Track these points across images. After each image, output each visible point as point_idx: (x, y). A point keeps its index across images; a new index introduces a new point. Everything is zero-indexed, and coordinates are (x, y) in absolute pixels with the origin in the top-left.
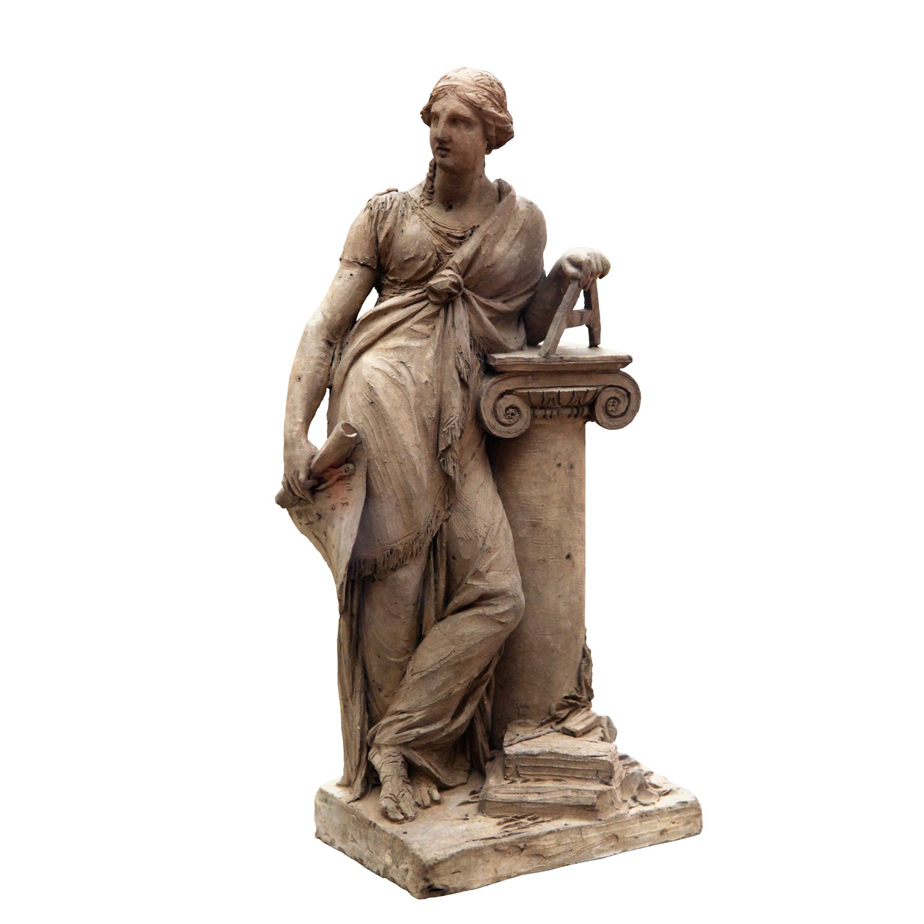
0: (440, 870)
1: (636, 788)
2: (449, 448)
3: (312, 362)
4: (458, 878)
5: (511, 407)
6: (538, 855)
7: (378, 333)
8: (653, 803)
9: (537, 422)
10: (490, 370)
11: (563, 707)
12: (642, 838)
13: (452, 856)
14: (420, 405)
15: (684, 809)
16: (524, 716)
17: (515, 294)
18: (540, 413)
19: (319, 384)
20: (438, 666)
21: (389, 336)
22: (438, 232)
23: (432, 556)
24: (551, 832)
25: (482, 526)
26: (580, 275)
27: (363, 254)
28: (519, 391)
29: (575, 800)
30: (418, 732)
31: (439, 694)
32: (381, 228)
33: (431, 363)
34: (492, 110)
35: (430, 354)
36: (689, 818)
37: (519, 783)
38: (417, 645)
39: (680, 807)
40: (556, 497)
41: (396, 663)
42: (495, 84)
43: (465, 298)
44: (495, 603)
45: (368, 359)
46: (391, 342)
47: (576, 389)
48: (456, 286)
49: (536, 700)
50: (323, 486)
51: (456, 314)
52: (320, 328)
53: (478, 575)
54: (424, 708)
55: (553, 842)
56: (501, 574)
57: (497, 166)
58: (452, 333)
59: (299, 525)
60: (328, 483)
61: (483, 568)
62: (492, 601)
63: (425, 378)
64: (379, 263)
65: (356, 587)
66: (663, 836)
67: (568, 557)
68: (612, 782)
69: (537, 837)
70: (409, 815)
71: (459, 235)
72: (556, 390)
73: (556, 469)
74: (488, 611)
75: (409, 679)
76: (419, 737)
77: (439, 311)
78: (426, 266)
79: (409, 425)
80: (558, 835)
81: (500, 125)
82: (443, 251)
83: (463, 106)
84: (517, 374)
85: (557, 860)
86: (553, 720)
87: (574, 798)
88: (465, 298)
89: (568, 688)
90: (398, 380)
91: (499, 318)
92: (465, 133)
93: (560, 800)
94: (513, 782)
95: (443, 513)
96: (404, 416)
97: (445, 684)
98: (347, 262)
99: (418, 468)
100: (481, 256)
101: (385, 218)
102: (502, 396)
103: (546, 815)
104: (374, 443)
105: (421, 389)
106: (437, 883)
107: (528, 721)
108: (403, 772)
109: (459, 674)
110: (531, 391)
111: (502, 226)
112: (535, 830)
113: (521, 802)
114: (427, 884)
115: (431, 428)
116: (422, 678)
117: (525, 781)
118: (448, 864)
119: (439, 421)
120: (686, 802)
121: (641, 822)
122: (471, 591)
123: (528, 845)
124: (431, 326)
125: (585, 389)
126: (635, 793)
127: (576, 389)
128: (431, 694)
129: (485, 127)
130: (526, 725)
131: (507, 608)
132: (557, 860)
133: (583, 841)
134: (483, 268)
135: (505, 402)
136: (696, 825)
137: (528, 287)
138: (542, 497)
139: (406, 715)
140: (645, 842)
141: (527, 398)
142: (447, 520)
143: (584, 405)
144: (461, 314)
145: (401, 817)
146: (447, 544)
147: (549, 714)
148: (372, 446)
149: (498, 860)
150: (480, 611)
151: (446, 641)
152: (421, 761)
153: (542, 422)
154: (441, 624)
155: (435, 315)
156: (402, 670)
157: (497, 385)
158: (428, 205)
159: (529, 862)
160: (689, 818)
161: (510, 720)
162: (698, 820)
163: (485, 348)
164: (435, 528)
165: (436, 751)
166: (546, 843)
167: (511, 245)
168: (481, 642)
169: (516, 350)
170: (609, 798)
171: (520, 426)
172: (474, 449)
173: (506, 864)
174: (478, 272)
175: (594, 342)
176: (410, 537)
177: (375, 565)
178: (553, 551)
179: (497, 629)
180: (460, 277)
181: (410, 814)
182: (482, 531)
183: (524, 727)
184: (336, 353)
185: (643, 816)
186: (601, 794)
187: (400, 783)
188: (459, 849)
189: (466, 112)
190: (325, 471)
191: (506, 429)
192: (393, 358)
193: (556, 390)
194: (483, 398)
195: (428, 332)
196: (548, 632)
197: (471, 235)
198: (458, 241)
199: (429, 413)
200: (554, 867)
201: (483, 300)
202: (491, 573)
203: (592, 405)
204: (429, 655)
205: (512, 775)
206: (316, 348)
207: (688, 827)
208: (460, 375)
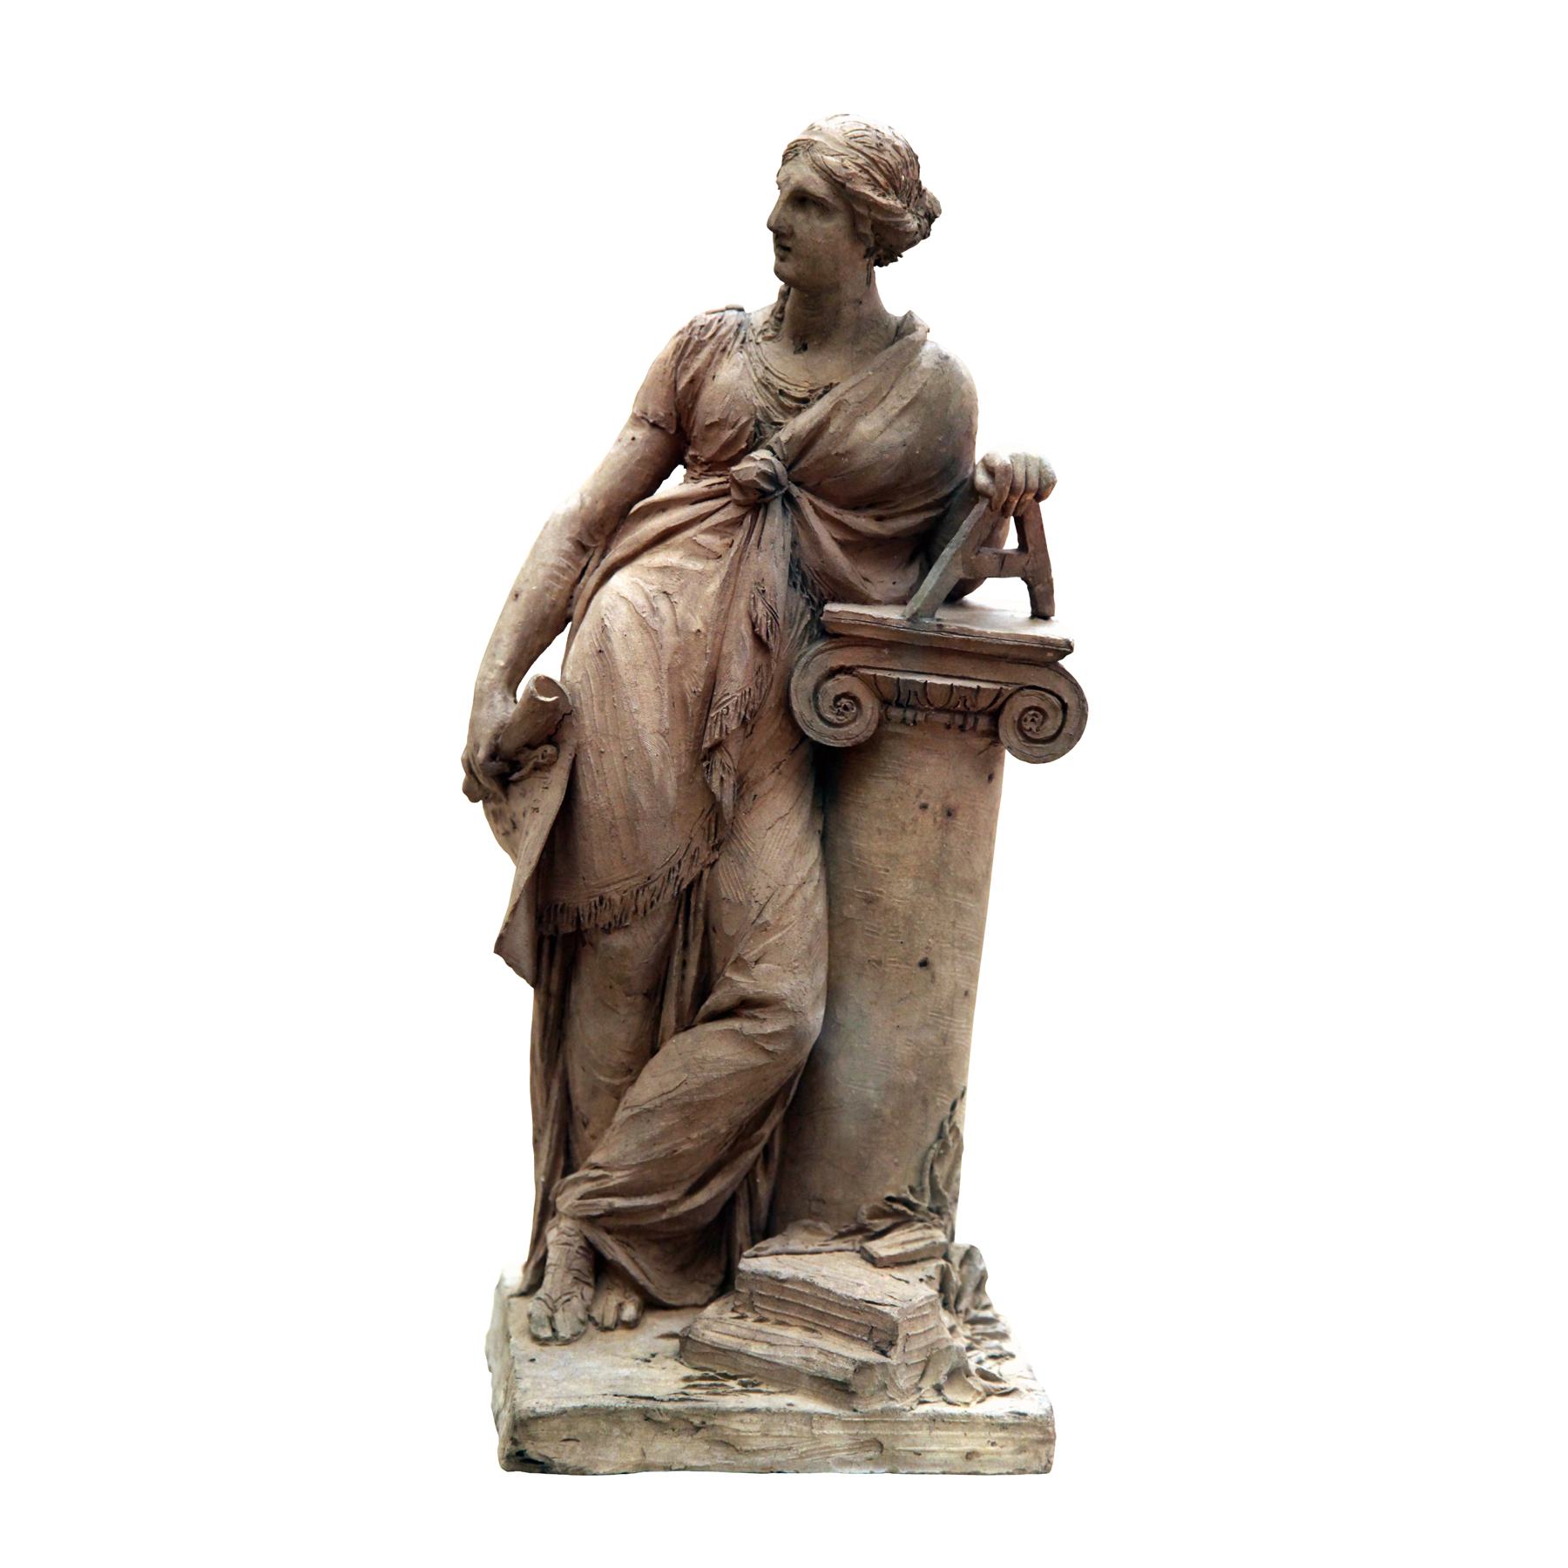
0: (540, 1429)
1: (946, 1370)
2: (717, 746)
3: (541, 572)
4: (573, 1450)
5: (845, 695)
6: (727, 1444)
7: (645, 540)
8: (967, 1404)
9: (891, 728)
10: (824, 632)
11: (878, 1213)
12: (929, 1456)
13: (564, 1411)
14: (681, 667)
15: (1019, 1425)
16: (816, 1216)
17: (904, 508)
18: (895, 713)
19: (547, 610)
20: (658, 1102)
21: (661, 546)
22: (766, 385)
23: (681, 921)
24: (752, 1411)
25: (763, 884)
26: (992, 490)
27: (658, 410)
28: (862, 671)
29: (820, 1368)
30: (610, 1204)
31: (656, 1149)
32: (686, 368)
33: (712, 601)
34: (867, 190)
35: (713, 586)
36: (1032, 1443)
37: (749, 1322)
38: (644, 1062)
39: (1010, 1420)
40: (912, 860)
41: (608, 1086)
42: (888, 146)
43: (789, 500)
44: (762, 1016)
45: (620, 580)
46: (660, 557)
47: (957, 683)
48: (772, 478)
49: (838, 1194)
50: (516, 776)
51: (767, 526)
52: (570, 519)
53: (741, 965)
54: (629, 1167)
55: (757, 1427)
56: (783, 968)
57: (898, 287)
58: (753, 555)
59: (496, 833)
60: (523, 772)
61: (750, 955)
62: (757, 1012)
63: (697, 624)
64: (678, 426)
65: (558, 949)
66: (970, 1463)
67: (924, 964)
68: (891, 1352)
69: (726, 1413)
70: (561, 1334)
71: (799, 395)
72: (920, 679)
73: (918, 813)
74: (748, 1027)
75: (621, 1115)
76: (612, 1213)
77: (743, 517)
78: (735, 440)
79: (653, 699)
80: (766, 1419)
81: (880, 217)
82: (767, 417)
83: (815, 176)
84: (862, 642)
85: (761, 1460)
86: (858, 1232)
87: (820, 1364)
88: (789, 500)
89: (897, 1182)
90: (650, 621)
91: (856, 544)
92: (817, 223)
93: (796, 1363)
94: (742, 1317)
95: (704, 855)
96: (647, 681)
97: (665, 1134)
98: (638, 419)
99: (656, 770)
100: (826, 436)
101: (696, 351)
102: (832, 673)
103: (771, 1382)
104: (591, 718)
105: (687, 643)
106: (532, 1450)
107: (821, 1225)
108: (580, 1263)
109: (689, 1123)
110: (880, 674)
111: (878, 390)
112: (730, 1402)
113: (739, 1352)
114: (515, 1449)
115: (694, 709)
116: (633, 1117)
117: (761, 1320)
118: (555, 1423)
119: (708, 698)
120: (1025, 1415)
121: (930, 1429)
122: (727, 989)
123: (709, 1423)
124: (728, 541)
125: (974, 685)
126: (942, 1380)
127: (957, 683)
128: (642, 1145)
129: (854, 219)
130: (817, 1231)
131: (778, 1028)
132: (761, 1460)
133: (814, 1437)
134: (828, 455)
135: (833, 687)
136: (1037, 1455)
137: (929, 500)
138: (887, 855)
139: (600, 1172)
140: (934, 1465)
141: (873, 684)
142: (712, 865)
143: (980, 712)
144: (776, 525)
145: (547, 1333)
146: (707, 906)
147: (855, 1219)
148: (587, 722)
149: (650, 1436)
150: (735, 1024)
151: (678, 1064)
152: (615, 1252)
153: (899, 729)
154: (682, 1036)
155: (736, 523)
156: (618, 1094)
157: (825, 656)
158: (770, 339)
159: (708, 1451)
160: (1032, 1443)
161: (796, 1218)
162: (1043, 1450)
163: (815, 584)
164: (686, 875)
165: (657, 1242)
166: (742, 1427)
167: (889, 424)
168: (731, 1076)
169: (888, 603)
170: (878, 1377)
171: (858, 729)
172: (781, 755)
173: (663, 1446)
174: (819, 460)
175: (1041, 609)
176: (632, 882)
177: (578, 919)
178: (908, 944)
179: (761, 1060)
180: (779, 467)
181: (564, 1332)
182: (762, 894)
183: (811, 1232)
184: (592, 563)
185: (935, 1420)
186: (862, 1367)
187: (569, 1280)
188: (579, 1404)
189: (819, 187)
190: (518, 751)
191: (832, 729)
192: (653, 583)
193: (920, 679)
194: (796, 674)
195: (719, 550)
196: (870, 1084)
197: (820, 397)
198: (794, 404)
199: (693, 684)
200: (752, 1469)
201: (830, 510)
202: (763, 966)
203: (995, 715)
204: (653, 1083)
205: (744, 1305)
206: (555, 552)
207: (1022, 1457)
208: (754, 626)
